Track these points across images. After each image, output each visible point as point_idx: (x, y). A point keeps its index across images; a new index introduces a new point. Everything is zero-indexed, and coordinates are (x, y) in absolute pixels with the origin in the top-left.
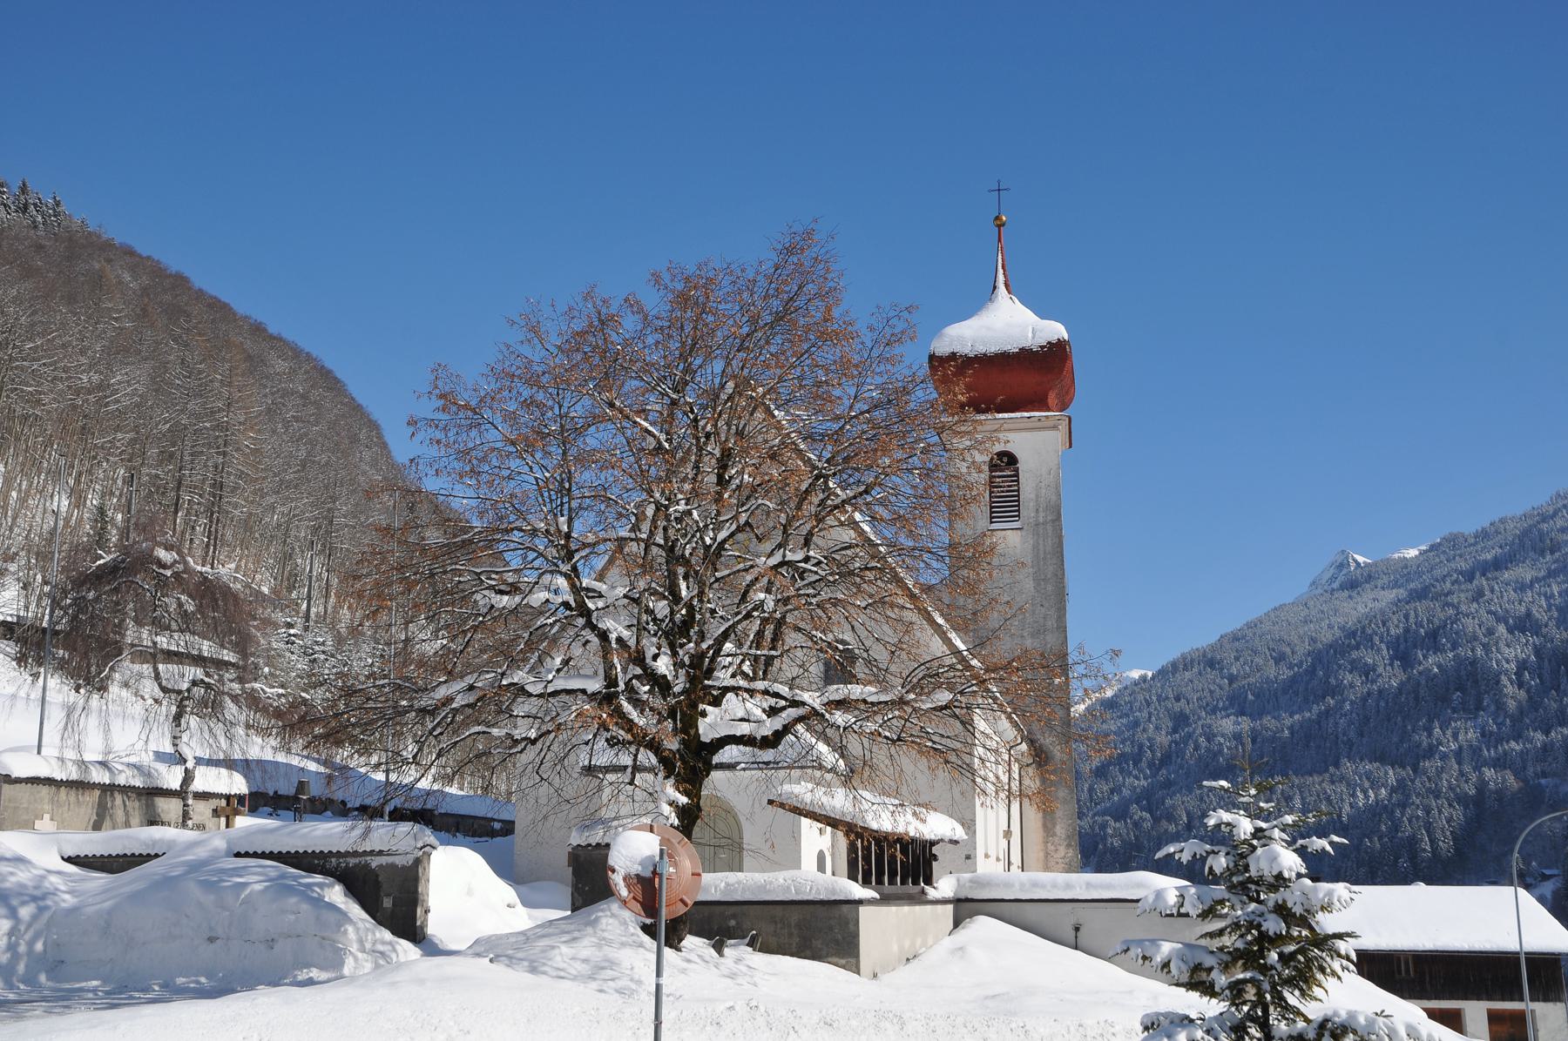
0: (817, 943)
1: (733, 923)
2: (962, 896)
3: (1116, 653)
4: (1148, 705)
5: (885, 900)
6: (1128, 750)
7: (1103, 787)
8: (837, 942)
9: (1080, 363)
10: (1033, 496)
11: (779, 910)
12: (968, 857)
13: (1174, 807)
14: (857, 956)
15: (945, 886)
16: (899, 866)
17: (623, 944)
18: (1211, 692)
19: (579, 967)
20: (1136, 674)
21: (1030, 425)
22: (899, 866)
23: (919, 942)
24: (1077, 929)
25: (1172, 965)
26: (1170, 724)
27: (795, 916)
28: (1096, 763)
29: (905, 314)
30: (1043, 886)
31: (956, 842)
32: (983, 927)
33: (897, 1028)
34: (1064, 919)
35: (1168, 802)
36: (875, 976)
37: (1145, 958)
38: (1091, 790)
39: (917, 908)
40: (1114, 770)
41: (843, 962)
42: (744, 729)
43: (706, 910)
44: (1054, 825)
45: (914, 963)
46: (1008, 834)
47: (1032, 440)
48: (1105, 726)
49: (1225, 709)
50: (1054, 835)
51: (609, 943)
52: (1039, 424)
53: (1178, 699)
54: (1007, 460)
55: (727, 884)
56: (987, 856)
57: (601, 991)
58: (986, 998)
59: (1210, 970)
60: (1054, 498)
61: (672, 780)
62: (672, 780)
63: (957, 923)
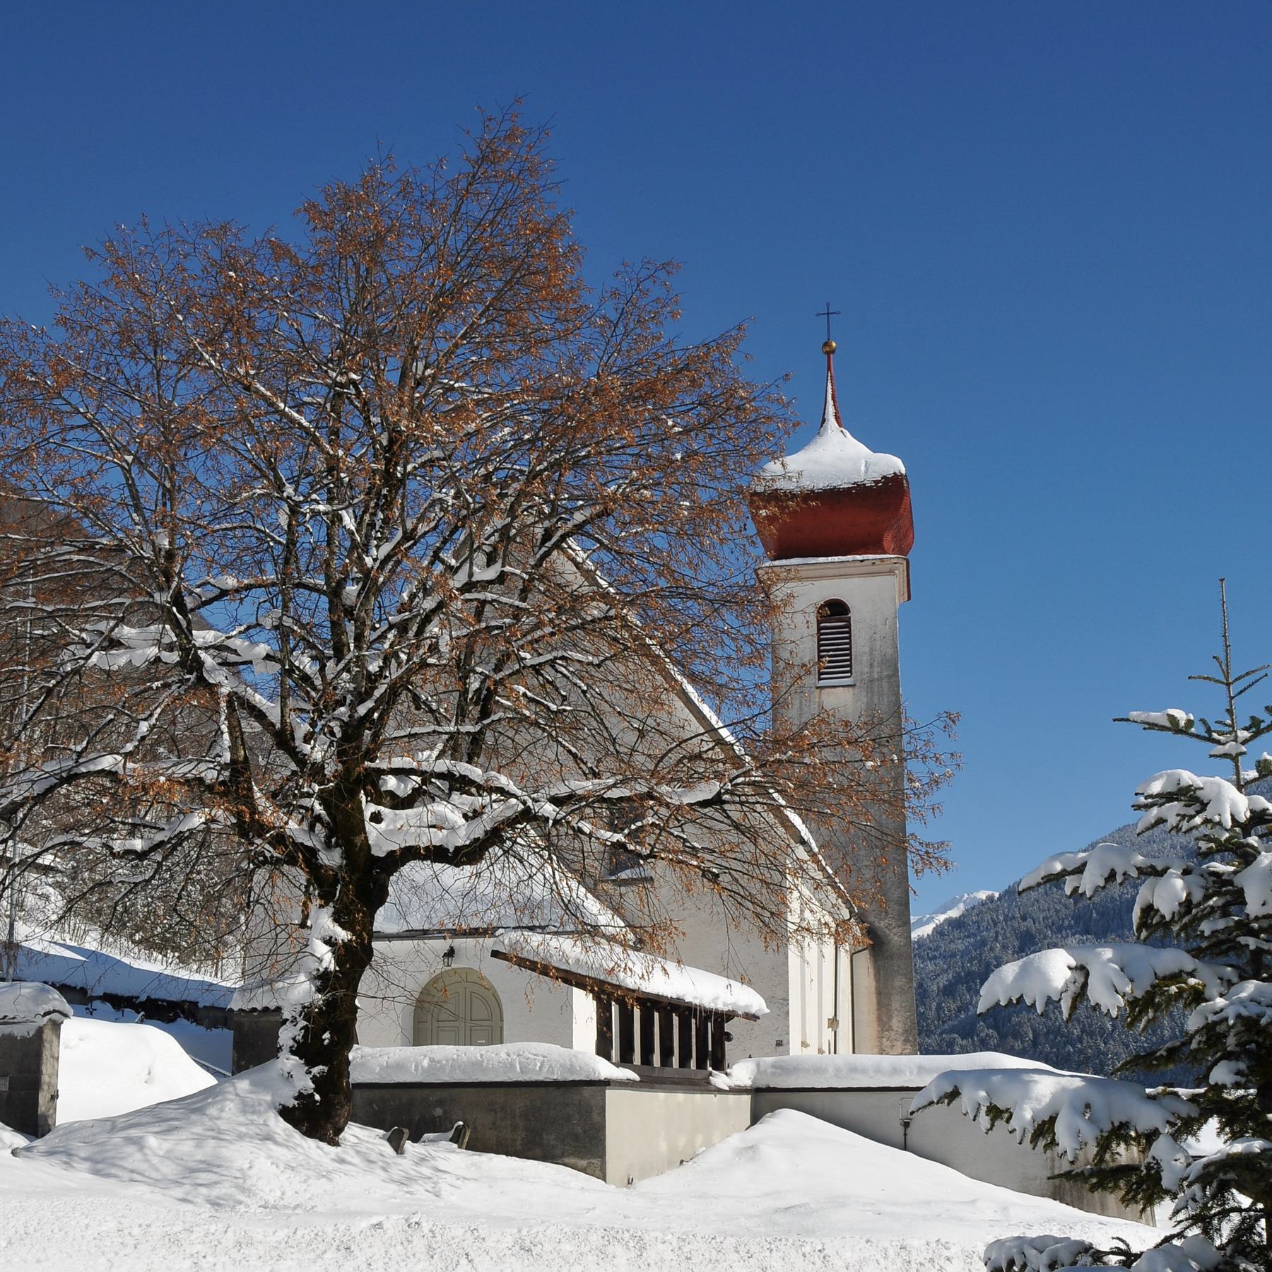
0: (550, 1139)
1: (439, 1112)
2: (762, 1084)
3: (952, 719)
4: (995, 924)
5: (649, 1082)
6: (975, 968)
7: (951, 1005)
8: (576, 1137)
9: (919, 500)
10: (867, 649)
11: (499, 1094)
12: (779, 1044)
13: (1020, 1024)
14: (602, 1155)
15: (742, 1072)
16: (677, 1044)
17: (241, 1137)
18: (1056, 911)
19: (168, 1169)
20: (983, 895)
21: (863, 570)
22: (677, 1044)
23: (699, 1139)
24: (906, 1125)
25: (1060, 1129)
26: (1016, 943)
27: (520, 1102)
28: (943, 981)
29: (662, 275)
30: (864, 1071)
31: (754, 1017)
32: (788, 1121)
33: (633, 1254)
34: (890, 1112)
35: (1015, 1019)
36: (630, 1182)
37: (996, 1113)
38: (939, 1008)
39: (698, 1097)
40: (962, 989)
41: (584, 1163)
42: (438, 838)
43: (405, 1095)
44: (890, 1018)
45: (145, 1076)
46: (834, 1023)
47: (868, 588)
48: (952, 946)
49: (1070, 927)
50: (890, 1028)
51: (218, 1135)
52: (874, 568)
53: (1024, 918)
54: (836, 610)
55: (432, 1060)
56: (804, 1044)
57: (184, 1200)
58: (777, 1210)
59: (1151, 1137)
60: (890, 651)
61: (330, 910)
62: (330, 910)
63: (755, 1118)
